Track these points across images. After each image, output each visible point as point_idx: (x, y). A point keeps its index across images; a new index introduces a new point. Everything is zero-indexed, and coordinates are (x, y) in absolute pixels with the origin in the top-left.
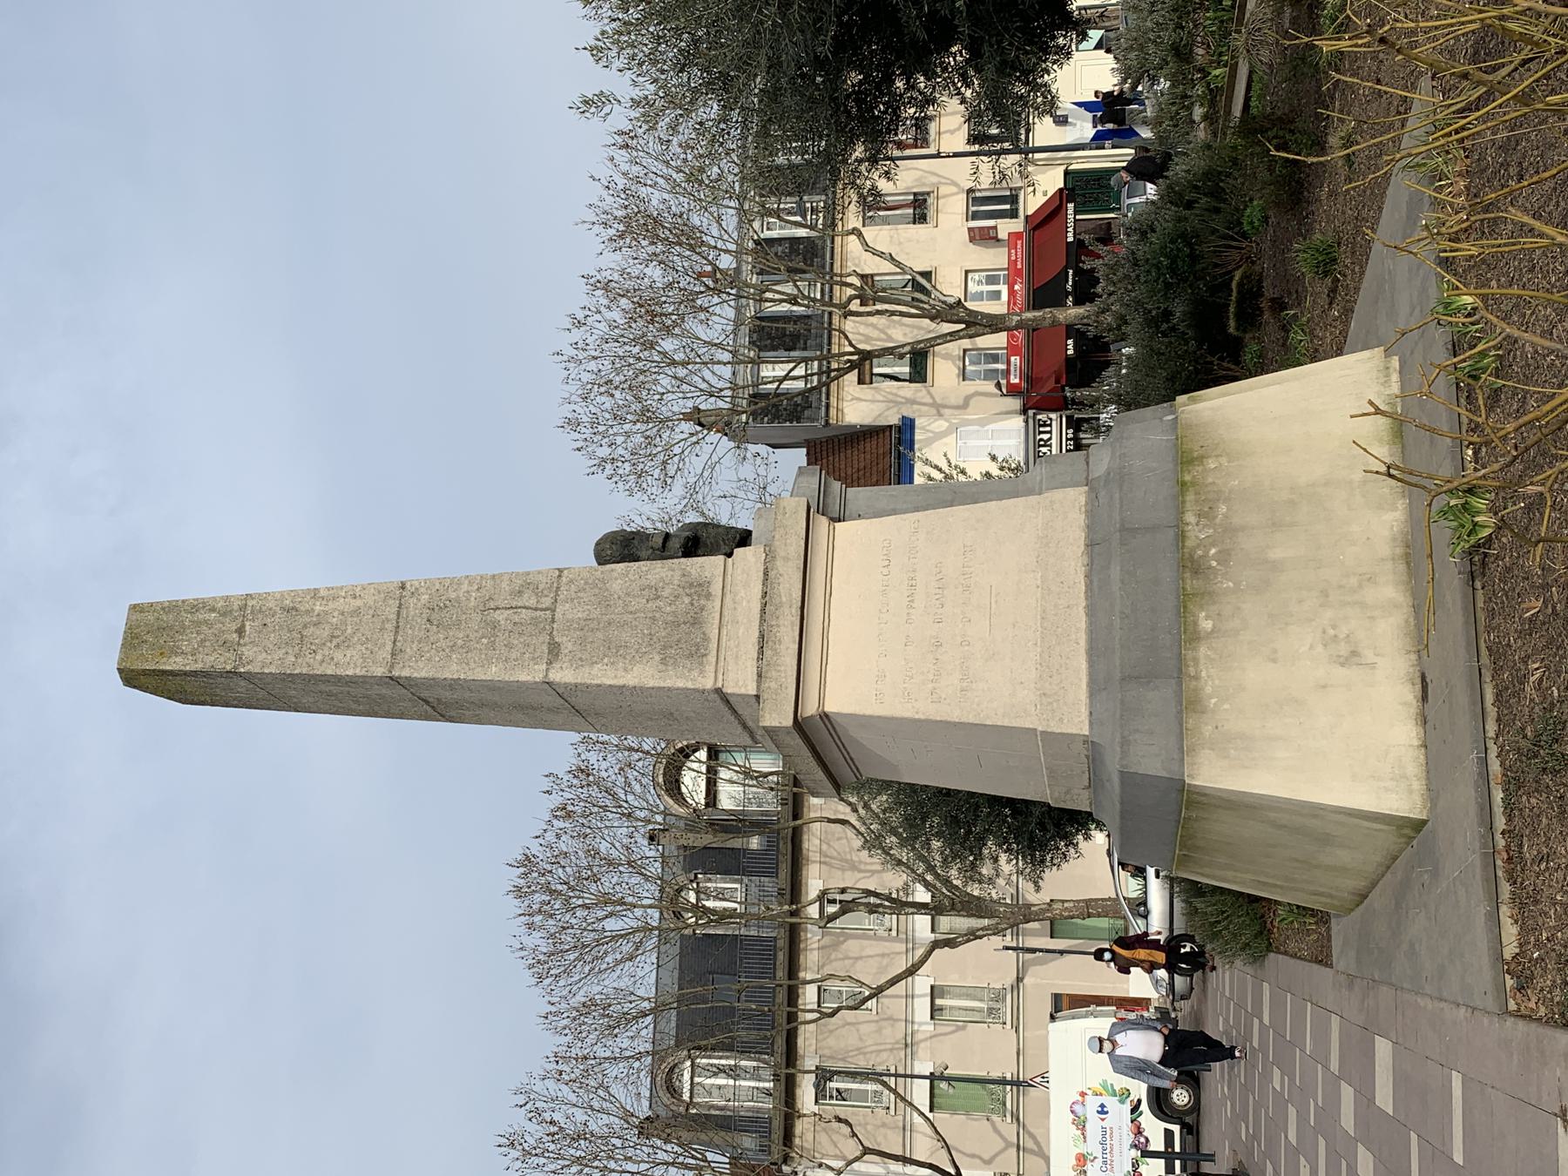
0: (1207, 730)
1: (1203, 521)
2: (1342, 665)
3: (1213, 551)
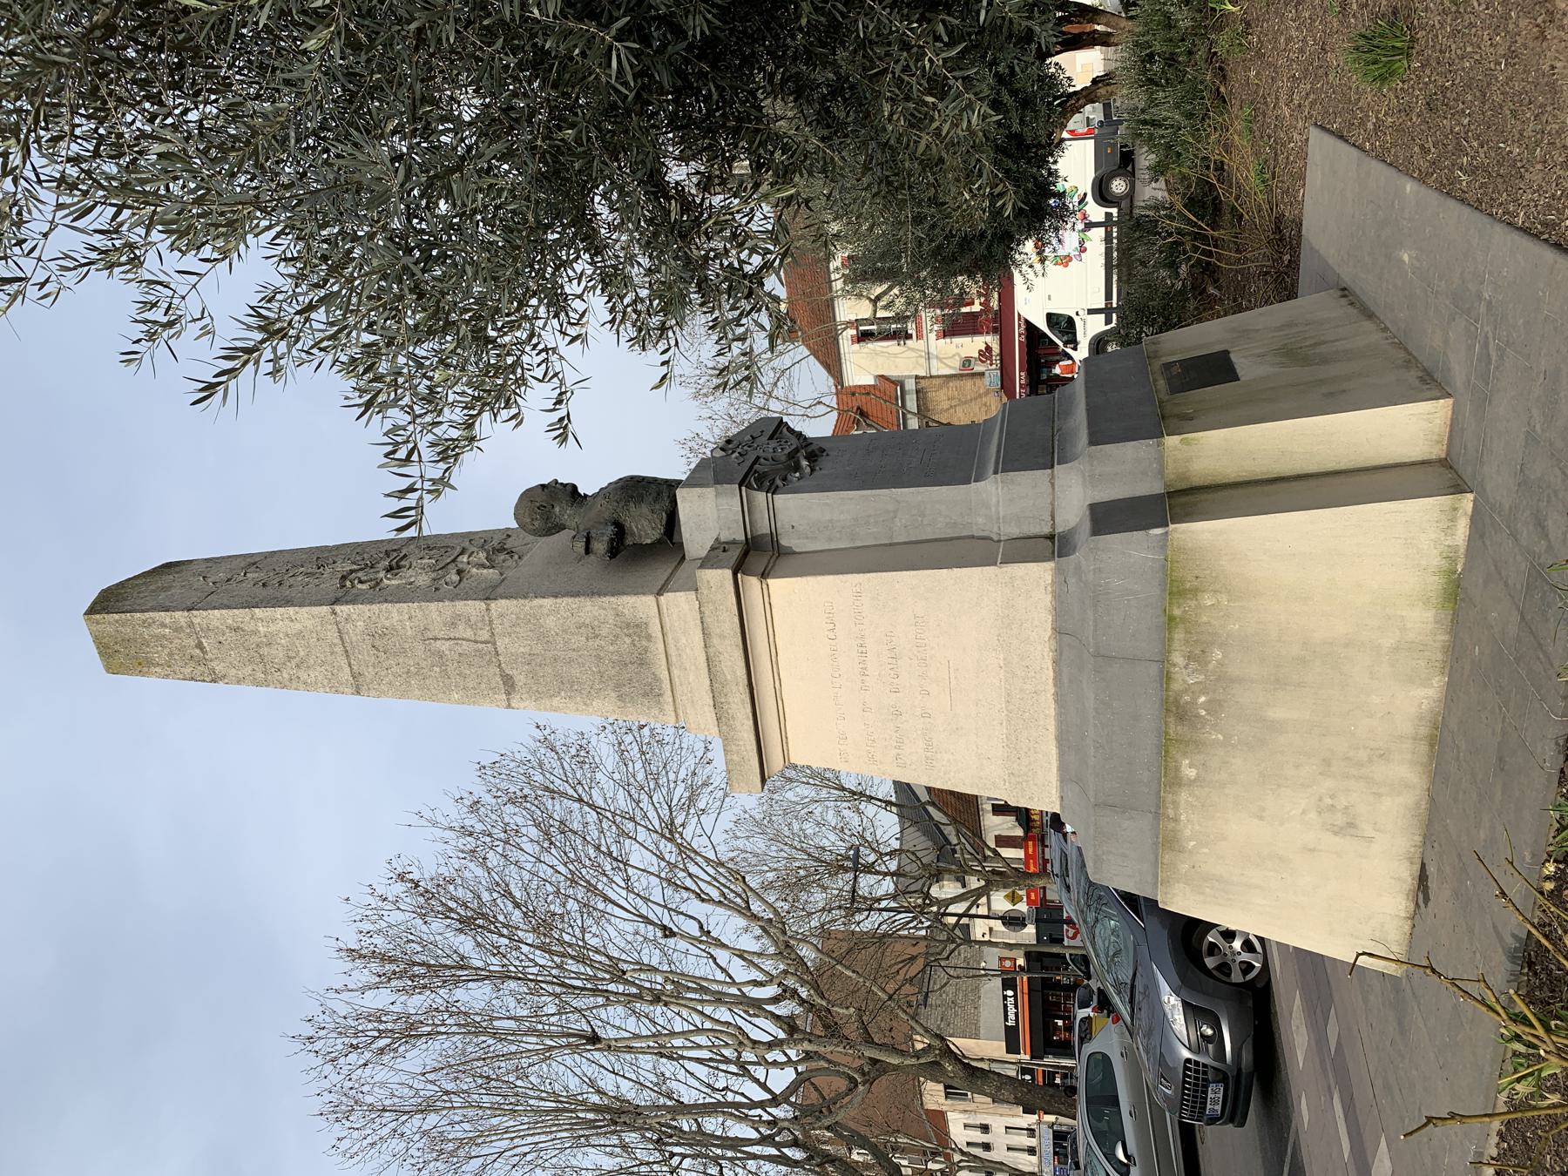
0: (1184, 867)
1: (1193, 665)
2: (1336, 833)
3: (1202, 699)
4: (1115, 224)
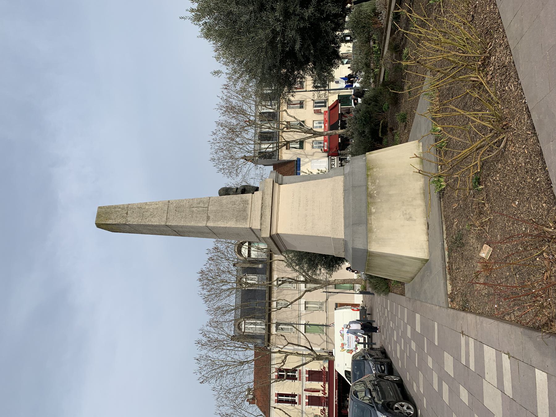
0: (374, 237)
4: (367, 343)
